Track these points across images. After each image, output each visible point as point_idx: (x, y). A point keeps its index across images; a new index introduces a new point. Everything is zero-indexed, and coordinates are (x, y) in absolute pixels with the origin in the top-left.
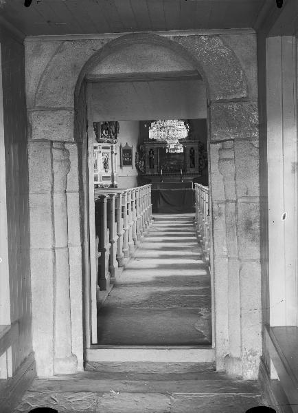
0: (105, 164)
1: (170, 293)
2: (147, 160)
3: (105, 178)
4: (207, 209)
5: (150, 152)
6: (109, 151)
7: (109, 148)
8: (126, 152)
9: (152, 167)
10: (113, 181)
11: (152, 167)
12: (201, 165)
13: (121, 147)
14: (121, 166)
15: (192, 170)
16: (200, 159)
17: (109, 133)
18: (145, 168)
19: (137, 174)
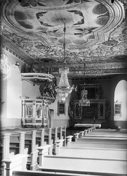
0: (38, 112)
1: (121, 74)
2: (75, 111)
3: (38, 121)
4: (104, 4)
5: (77, 106)
6: (42, 104)
7: (41, 102)
8: (61, 106)
9: (77, 115)
10: (43, 123)
11: (77, 115)
12: (115, 70)
13: (58, 102)
14: (58, 113)
15: (101, 117)
16: (106, 111)
17: (50, 94)
18: (74, 115)
19: (69, 119)
